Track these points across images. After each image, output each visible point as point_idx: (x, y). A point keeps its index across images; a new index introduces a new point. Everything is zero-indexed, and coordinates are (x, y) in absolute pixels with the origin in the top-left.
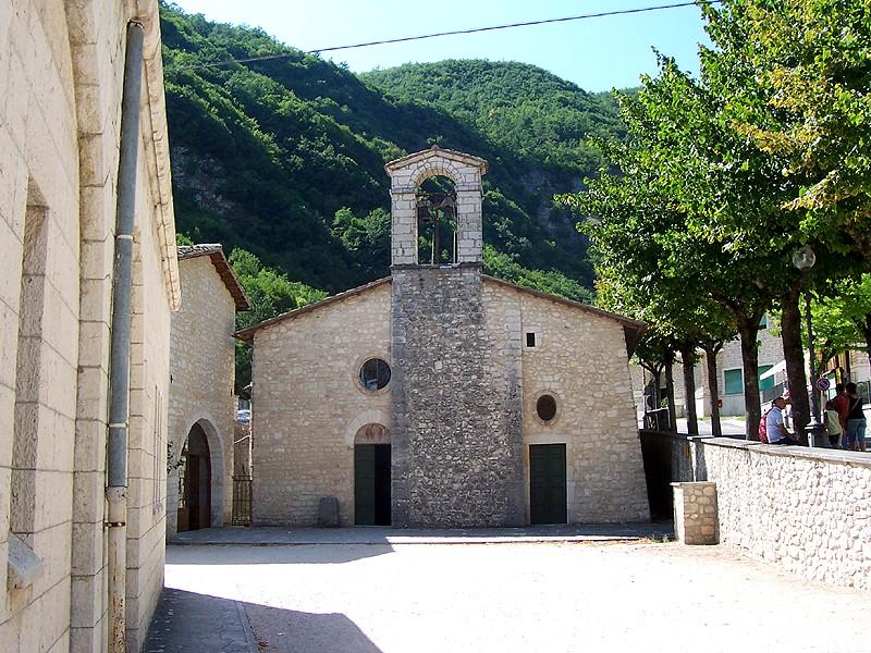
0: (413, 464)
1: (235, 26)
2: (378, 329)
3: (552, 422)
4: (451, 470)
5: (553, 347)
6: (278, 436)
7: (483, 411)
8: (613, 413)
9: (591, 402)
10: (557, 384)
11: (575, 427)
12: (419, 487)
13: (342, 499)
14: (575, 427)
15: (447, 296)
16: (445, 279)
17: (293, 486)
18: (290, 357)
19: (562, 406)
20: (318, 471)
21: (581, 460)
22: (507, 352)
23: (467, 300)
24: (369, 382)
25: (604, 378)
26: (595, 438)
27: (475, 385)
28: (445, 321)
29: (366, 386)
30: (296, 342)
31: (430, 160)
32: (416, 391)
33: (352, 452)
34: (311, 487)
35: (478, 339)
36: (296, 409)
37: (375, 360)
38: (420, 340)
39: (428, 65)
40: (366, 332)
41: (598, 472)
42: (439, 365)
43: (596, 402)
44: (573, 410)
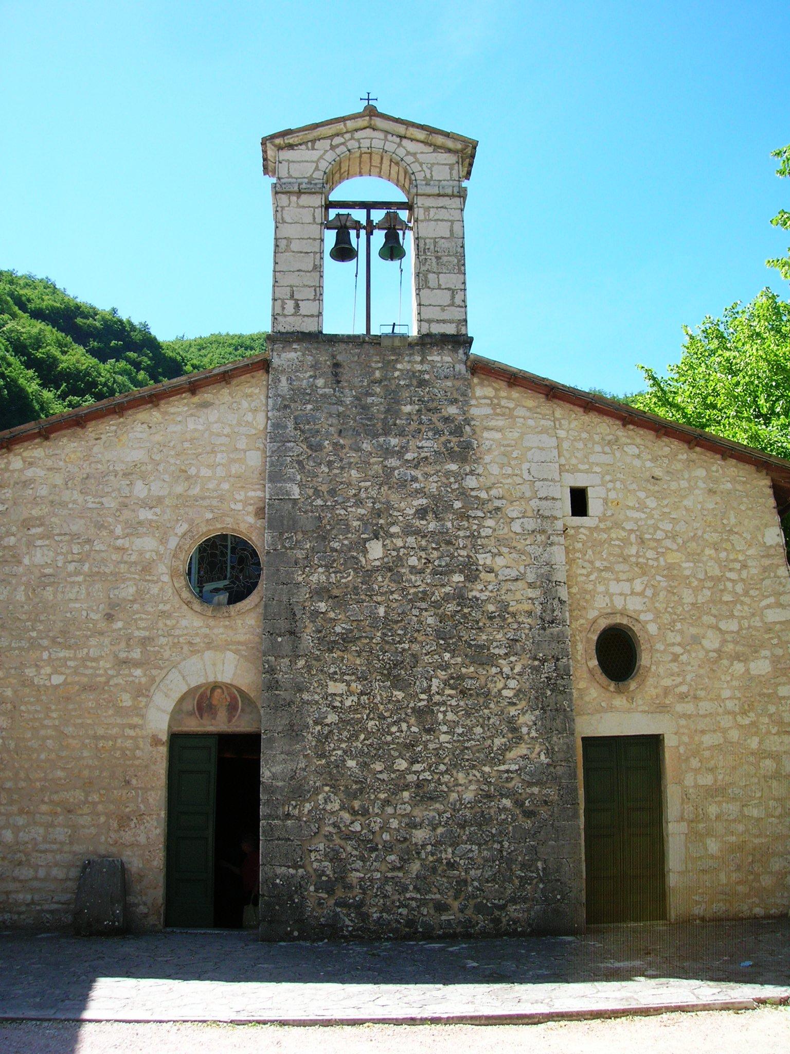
0: (313, 781)
1: (19, 274)
2: (235, 469)
3: (633, 685)
4: (406, 794)
5: (628, 519)
8: (761, 666)
9: (711, 641)
10: (638, 599)
11: (683, 697)
12: (329, 837)
13: (135, 864)
14: (683, 697)
15: (393, 400)
16: (389, 366)
17: (17, 829)
18: (27, 524)
19: (652, 650)
20: (80, 795)
21: (697, 771)
22: (531, 524)
23: (436, 410)
24: (208, 587)
25: (739, 588)
26: (726, 722)
27: (460, 597)
28: (387, 452)
29: (203, 597)
30: (43, 491)
31: (358, 135)
32: (322, 606)
33: (164, 750)
34: (61, 834)
35: (463, 494)
36: (34, 645)
37: (224, 537)
38: (333, 492)
39: (240, 336)
40: (205, 472)
41: (734, 799)
43: (724, 642)
44: (676, 658)
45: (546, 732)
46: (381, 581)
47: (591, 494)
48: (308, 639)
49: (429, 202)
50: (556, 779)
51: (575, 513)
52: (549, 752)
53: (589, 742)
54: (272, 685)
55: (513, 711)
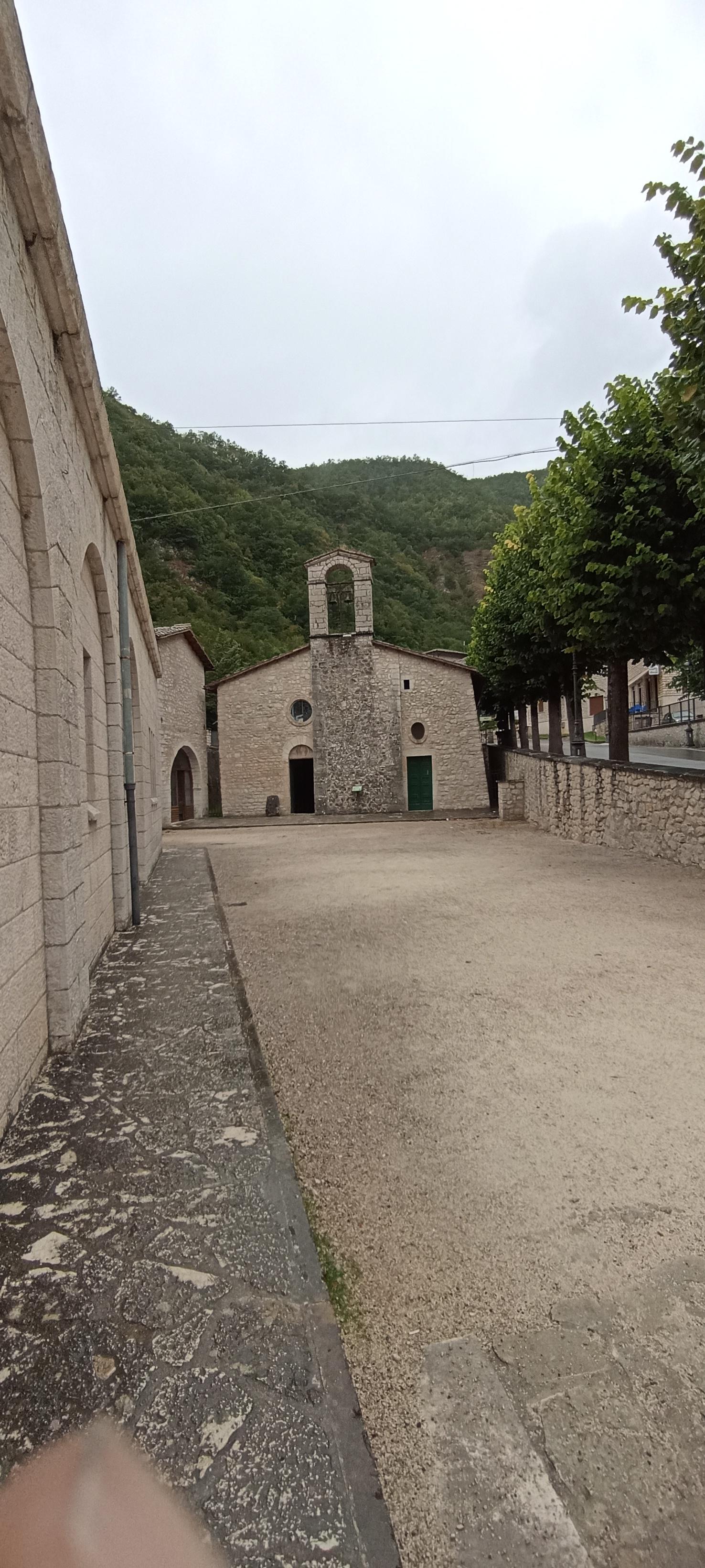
6: (237, 755)
7: (375, 734)
11: (438, 744)
22: (390, 693)
33: (288, 765)
35: (370, 684)
42: (344, 704)
45: (393, 756)
46: (346, 714)
47: (410, 682)
48: (326, 731)
49: (359, 583)
50: (396, 769)
51: (309, 763)
52: (394, 762)
53: (410, 759)
54: (316, 746)
55: (384, 750)
